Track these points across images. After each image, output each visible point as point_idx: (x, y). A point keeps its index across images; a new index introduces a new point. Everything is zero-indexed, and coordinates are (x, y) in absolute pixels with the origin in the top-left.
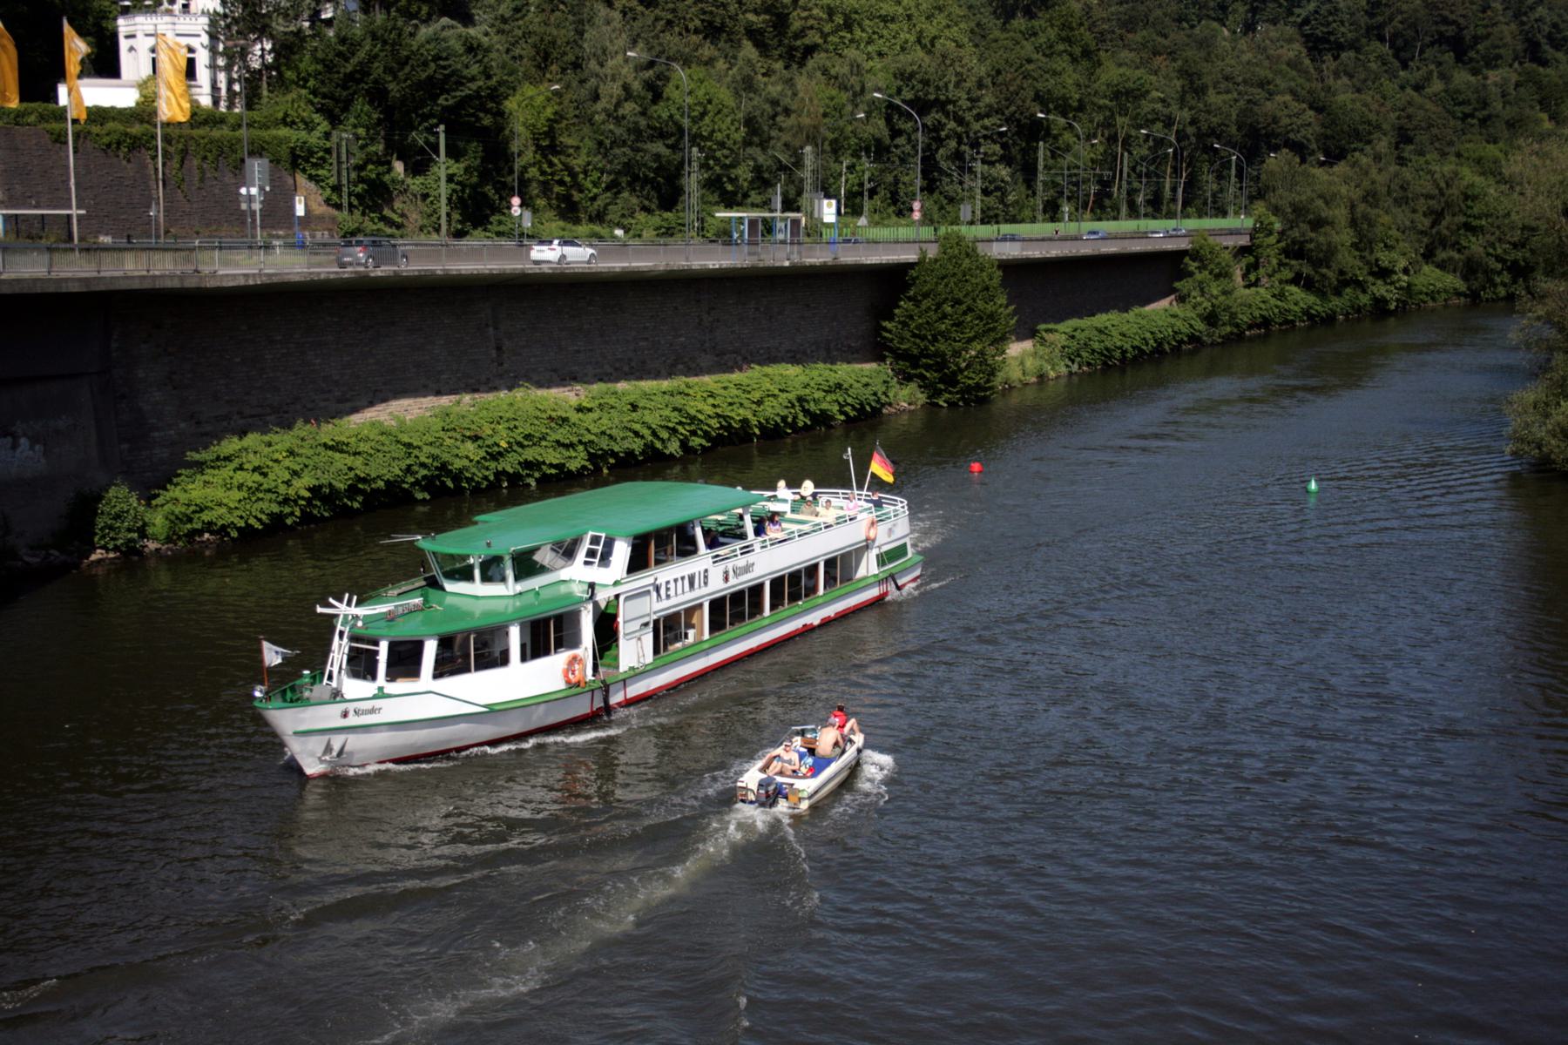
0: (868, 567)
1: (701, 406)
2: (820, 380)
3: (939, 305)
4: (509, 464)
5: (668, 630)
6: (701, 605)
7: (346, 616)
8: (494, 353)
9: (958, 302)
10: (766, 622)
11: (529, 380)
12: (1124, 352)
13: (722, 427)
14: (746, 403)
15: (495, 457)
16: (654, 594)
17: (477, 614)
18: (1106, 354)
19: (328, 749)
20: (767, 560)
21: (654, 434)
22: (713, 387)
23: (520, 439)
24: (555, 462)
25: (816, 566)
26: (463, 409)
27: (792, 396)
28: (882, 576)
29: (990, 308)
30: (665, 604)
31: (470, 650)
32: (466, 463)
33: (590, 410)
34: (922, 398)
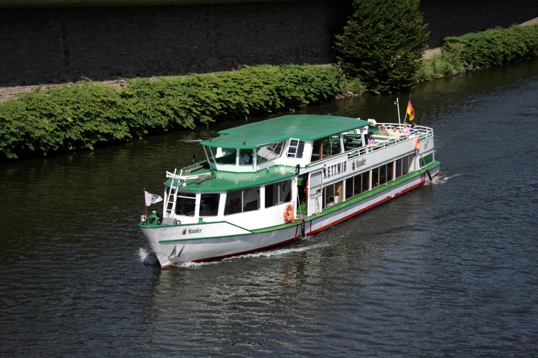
0: (415, 166)
1: (208, 93)
2: (292, 75)
3: (375, 24)
4: (74, 134)
5: (329, 193)
6: (342, 182)
7: (175, 180)
8: (63, 56)
9: (389, 21)
10: (370, 194)
11: (88, 75)
12: (505, 56)
13: (223, 108)
14: (239, 91)
15: (64, 128)
16: (323, 174)
17: (237, 182)
18: (493, 57)
19: (174, 251)
20: (373, 159)
21: (176, 113)
22: (217, 80)
23: (81, 116)
24: (106, 131)
25: (392, 163)
26: (40, 95)
27: (272, 87)
28: (423, 172)
29: (411, 25)
30: (328, 180)
31: (241, 200)
32: (43, 132)
33: (131, 96)
34: (363, 88)
